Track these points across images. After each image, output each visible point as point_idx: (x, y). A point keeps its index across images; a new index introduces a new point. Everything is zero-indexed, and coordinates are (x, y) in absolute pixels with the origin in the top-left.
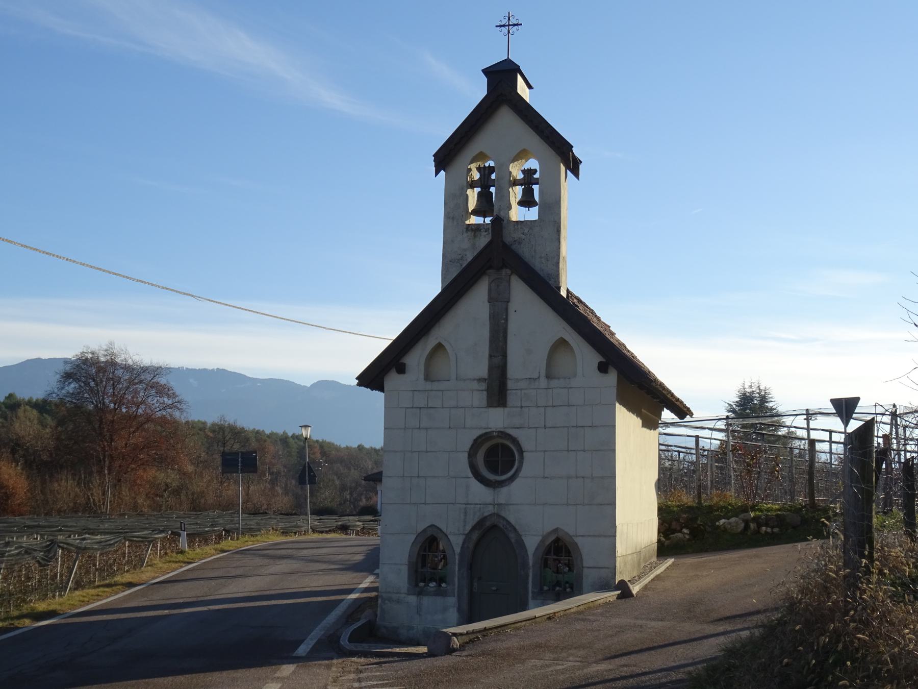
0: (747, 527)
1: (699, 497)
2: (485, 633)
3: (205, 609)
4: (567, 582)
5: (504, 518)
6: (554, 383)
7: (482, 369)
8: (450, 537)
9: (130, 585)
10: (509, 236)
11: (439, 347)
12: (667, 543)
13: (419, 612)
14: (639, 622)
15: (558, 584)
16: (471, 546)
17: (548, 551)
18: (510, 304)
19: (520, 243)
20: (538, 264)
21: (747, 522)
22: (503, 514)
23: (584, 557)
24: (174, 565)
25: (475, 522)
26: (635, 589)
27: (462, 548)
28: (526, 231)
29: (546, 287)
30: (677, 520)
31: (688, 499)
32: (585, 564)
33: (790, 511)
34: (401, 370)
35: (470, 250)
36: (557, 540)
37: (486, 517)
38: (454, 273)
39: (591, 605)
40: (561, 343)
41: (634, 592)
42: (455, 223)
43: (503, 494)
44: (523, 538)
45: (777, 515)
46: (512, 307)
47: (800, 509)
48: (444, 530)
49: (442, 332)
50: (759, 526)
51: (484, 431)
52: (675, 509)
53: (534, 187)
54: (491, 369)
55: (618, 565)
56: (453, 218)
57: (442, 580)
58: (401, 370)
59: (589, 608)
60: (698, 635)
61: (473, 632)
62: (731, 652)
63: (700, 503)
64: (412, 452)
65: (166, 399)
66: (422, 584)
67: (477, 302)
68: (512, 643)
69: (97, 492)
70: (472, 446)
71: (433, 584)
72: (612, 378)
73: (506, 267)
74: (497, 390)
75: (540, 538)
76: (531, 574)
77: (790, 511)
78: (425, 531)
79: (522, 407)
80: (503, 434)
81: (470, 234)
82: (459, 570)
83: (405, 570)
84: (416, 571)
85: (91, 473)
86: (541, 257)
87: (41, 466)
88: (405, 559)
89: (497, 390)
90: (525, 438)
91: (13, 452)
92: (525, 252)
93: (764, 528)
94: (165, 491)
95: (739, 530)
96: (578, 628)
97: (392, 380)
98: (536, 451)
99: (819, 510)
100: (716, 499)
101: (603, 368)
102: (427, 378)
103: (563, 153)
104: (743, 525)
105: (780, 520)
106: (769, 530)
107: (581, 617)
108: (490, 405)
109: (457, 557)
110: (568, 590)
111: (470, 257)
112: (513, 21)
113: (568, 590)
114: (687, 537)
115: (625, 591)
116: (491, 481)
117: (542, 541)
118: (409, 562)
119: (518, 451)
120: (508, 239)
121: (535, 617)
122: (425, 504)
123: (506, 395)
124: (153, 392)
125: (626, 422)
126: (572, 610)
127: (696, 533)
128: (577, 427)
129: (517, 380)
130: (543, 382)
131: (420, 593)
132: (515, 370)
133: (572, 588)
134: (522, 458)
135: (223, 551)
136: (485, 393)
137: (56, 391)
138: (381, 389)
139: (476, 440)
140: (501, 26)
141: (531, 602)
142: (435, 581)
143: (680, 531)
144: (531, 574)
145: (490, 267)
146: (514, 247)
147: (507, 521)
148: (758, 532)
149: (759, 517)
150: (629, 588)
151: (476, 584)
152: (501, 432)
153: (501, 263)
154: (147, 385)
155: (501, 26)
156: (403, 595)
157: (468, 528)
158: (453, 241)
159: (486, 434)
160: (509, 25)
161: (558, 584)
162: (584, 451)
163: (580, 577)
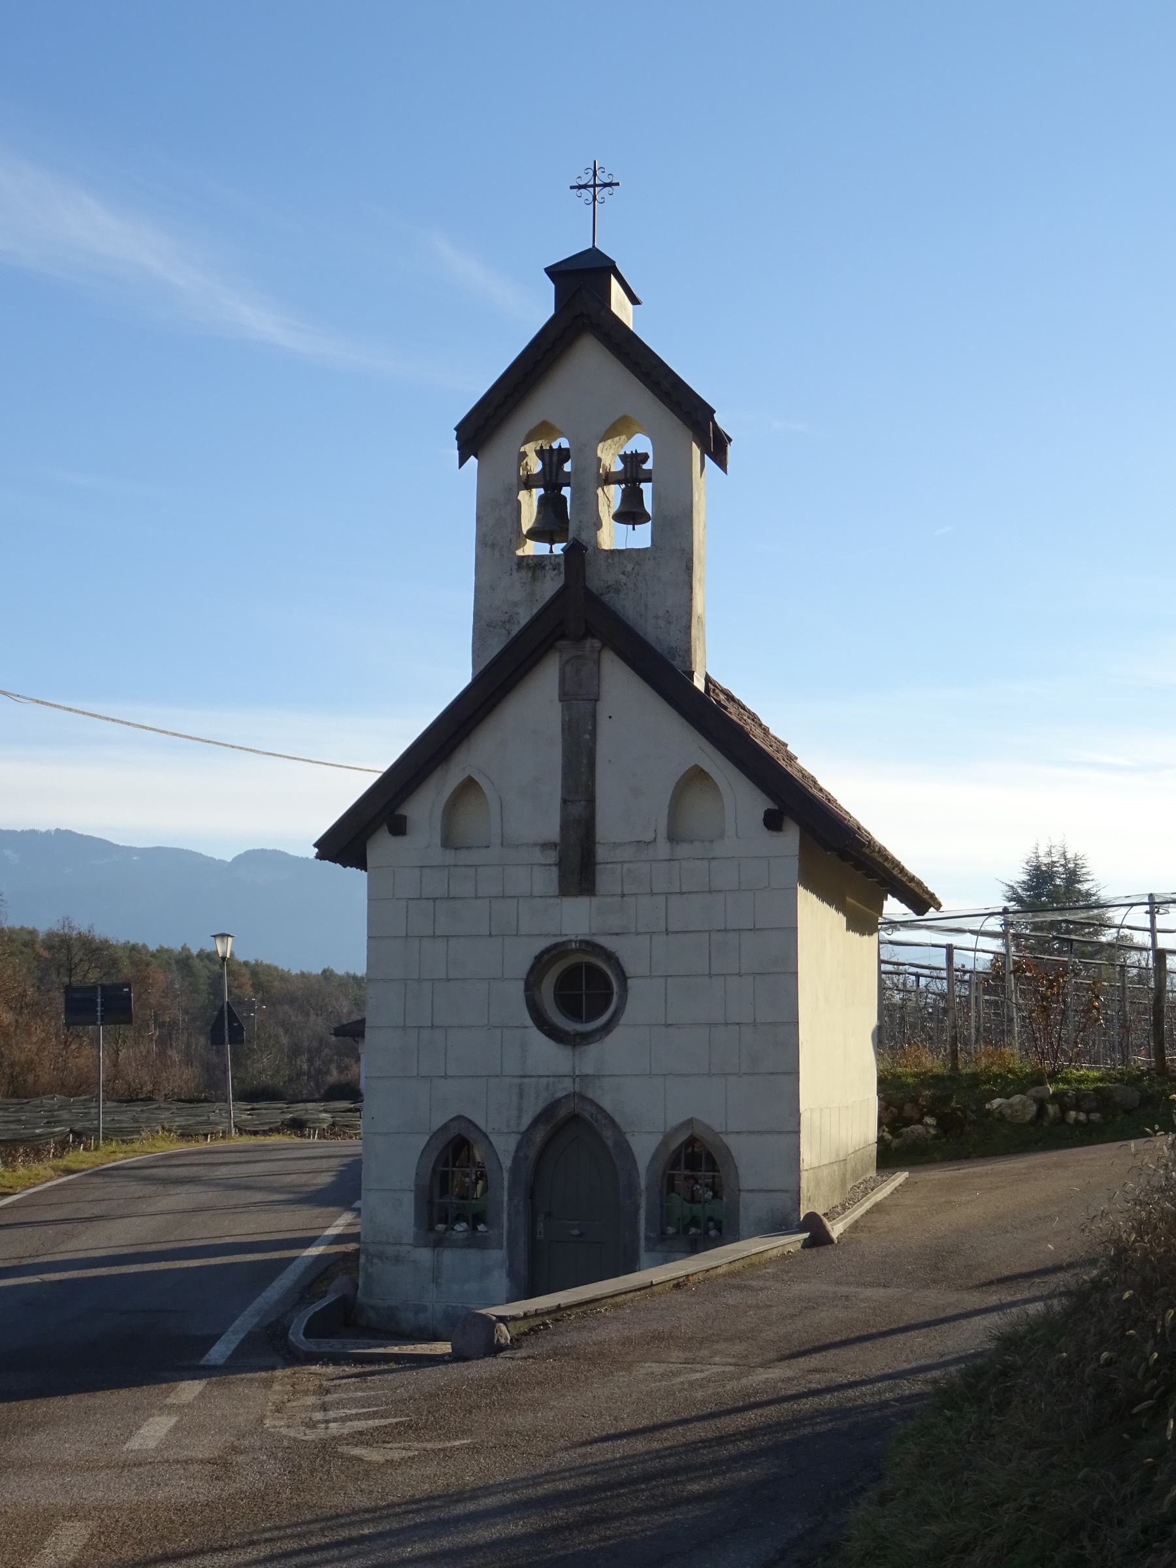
4: (710, 1219)
6: (683, 850)
7: (551, 829)
8: (492, 1138)
10: (598, 578)
11: (470, 784)
12: (896, 1143)
14: (844, 1290)
15: (694, 1222)
16: (532, 1154)
17: (674, 1163)
19: (618, 591)
20: (651, 631)
21: (1041, 1104)
22: (590, 1095)
25: (539, 1110)
26: (836, 1229)
28: (629, 568)
30: (914, 1101)
31: (933, 1062)
32: (744, 1185)
33: (1117, 1080)
34: (399, 828)
36: (692, 1141)
37: (558, 1101)
38: (496, 646)
39: (755, 1259)
40: (696, 776)
43: (592, 1057)
44: (628, 1137)
45: (1096, 1090)
46: (605, 708)
47: (1139, 1078)
49: (476, 757)
50: (1064, 1109)
52: (910, 1080)
53: (643, 486)
54: (565, 825)
55: (803, 1184)
57: (478, 1218)
58: (399, 828)
59: (752, 1265)
60: (950, 1312)
63: (955, 1068)
66: (440, 1227)
67: (539, 700)
68: (610, 1332)
71: (461, 1227)
72: (790, 839)
73: (593, 636)
74: (578, 862)
75: (660, 1138)
76: (643, 1203)
78: (445, 1127)
79: (623, 896)
80: (589, 946)
81: (526, 575)
82: (510, 1199)
84: (430, 1203)
86: (657, 617)
88: (409, 1182)
89: (578, 862)
92: (627, 606)
93: (1073, 1114)
95: (1028, 1117)
96: (730, 1302)
97: (382, 846)
98: (650, 977)
100: (984, 1061)
101: (773, 822)
102: (448, 842)
104: (1035, 1108)
105: (1102, 1100)
106: (1082, 1117)
107: (734, 1282)
108: (565, 891)
109: (506, 1176)
110: (713, 1233)
111: (524, 618)
112: (602, 178)
113: (713, 1233)
114: (933, 1131)
115: (817, 1236)
117: (664, 1143)
118: (417, 1186)
122: (445, 1077)
123: (593, 873)
125: (817, 921)
126: (720, 1271)
127: (948, 1124)
128: (726, 930)
129: (615, 845)
130: (663, 849)
131: (438, 1244)
133: (719, 1229)
135: (69, 1171)
136: (555, 869)
138: (362, 864)
139: (538, 959)
142: (466, 1220)
143: (920, 1121)
144: (643, 1203)
145: (563, 636)
148: (1061, 1120)
149: (1064, 1093)
150: (824, 1227)
152: (588, 943)
153: (581, 629)
156: (409, 1248)
157: (526, 1121)
159: (556, 945)
161: (694, 1222)
162: (740, 975)
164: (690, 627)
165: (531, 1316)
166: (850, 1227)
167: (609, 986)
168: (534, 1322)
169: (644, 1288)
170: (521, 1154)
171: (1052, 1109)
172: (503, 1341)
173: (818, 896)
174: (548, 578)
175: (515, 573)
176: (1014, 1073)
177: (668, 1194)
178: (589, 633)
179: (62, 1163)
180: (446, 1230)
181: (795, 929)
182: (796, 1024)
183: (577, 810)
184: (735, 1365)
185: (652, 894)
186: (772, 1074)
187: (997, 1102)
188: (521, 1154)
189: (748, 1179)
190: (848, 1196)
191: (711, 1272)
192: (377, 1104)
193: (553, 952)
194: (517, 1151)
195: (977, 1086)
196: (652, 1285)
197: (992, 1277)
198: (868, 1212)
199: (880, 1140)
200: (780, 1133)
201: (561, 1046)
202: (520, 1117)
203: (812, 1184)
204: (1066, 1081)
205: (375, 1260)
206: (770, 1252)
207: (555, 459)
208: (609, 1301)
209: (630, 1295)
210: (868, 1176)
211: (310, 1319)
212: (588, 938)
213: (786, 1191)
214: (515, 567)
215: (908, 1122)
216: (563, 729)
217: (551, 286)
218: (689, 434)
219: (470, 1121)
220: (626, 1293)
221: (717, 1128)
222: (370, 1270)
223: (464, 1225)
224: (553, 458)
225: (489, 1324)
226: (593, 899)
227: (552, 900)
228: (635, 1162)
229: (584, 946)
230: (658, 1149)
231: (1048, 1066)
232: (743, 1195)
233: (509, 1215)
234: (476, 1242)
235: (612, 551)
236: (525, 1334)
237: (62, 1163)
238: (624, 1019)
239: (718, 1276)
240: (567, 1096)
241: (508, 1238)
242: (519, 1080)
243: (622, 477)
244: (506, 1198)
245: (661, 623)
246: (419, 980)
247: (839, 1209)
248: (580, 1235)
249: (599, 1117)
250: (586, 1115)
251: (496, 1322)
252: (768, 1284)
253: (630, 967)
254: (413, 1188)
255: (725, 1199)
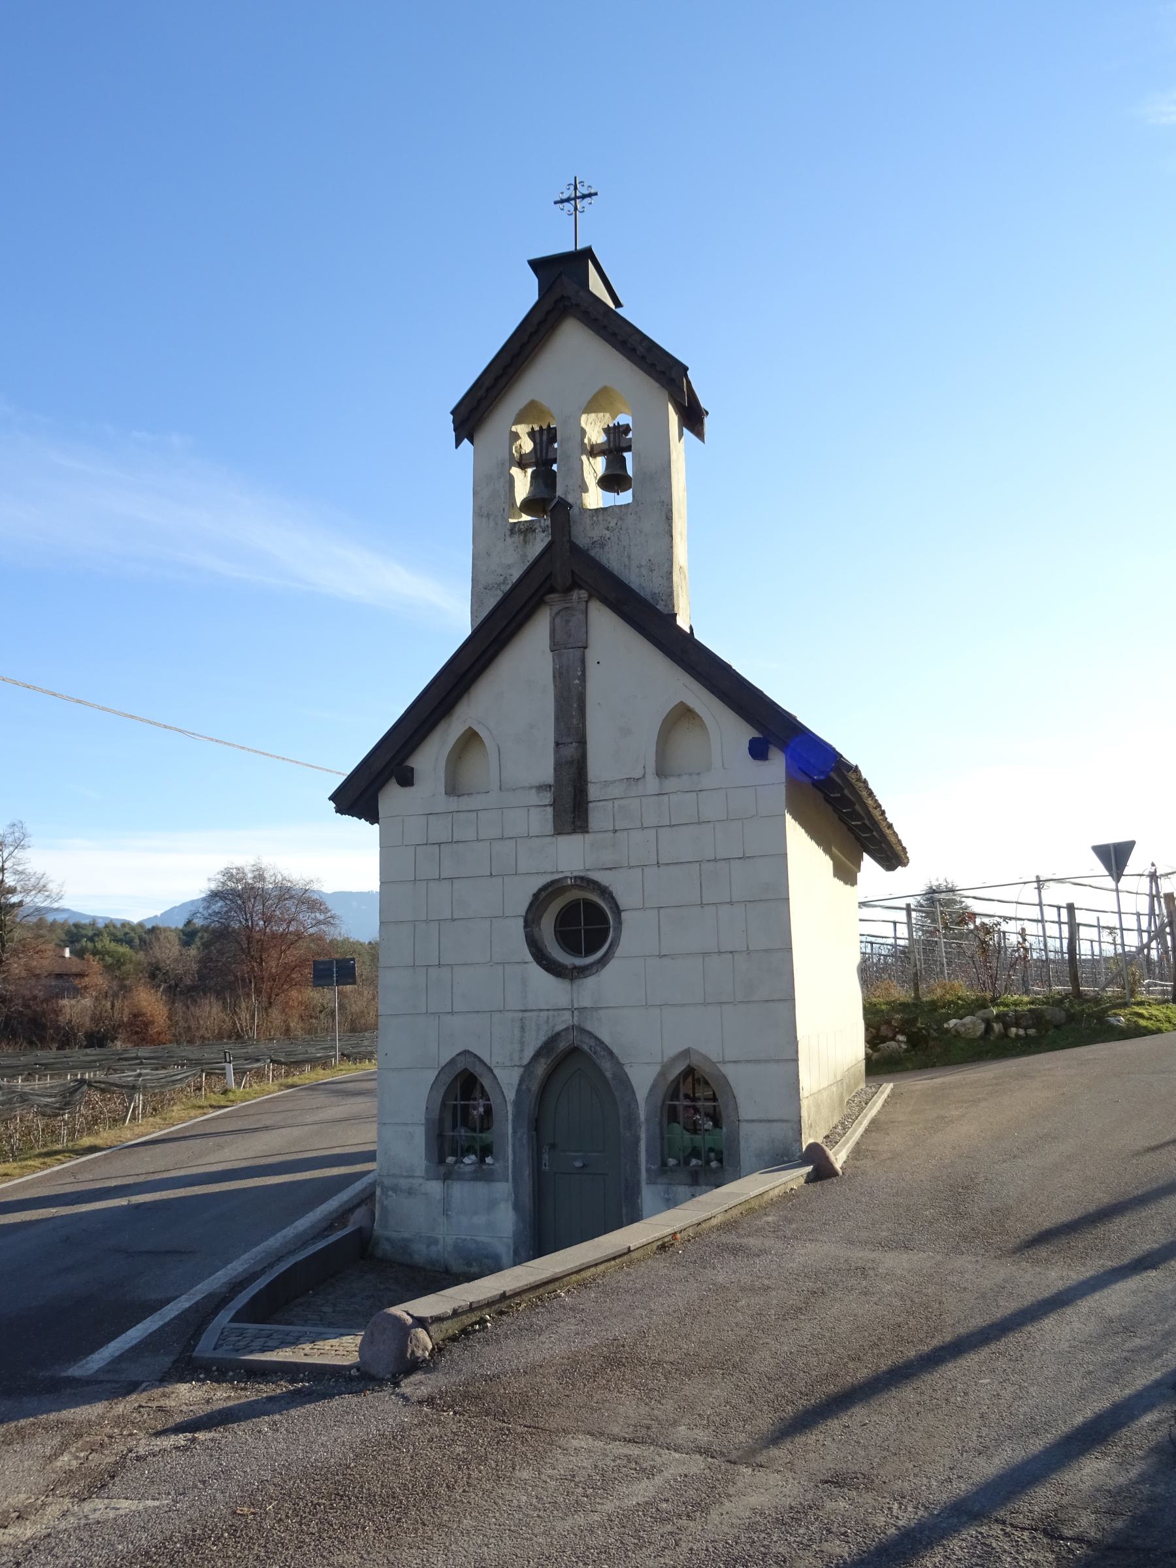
0: (988, 1029)
1: (917, 990)
2: (503, 1306)
3: (123, 1202)
4: (711, 1150)
5: (590, 1034)
6: (671, 784)
7: (546, 771)
8: (496, 1071)
9: (93, 1149)
10: (584, 535)
11: (471, 738)
12: (875, 1055)
13: (445, 1212)
14: (860, 1255)
15: (695, 1152)
16: (535, 1087)
17: (674, 1092)
18: (587, 651)
19: (602, 546)
20: (635, 579)
21: (988, 1023)
22: (589, 1027)
23: (741, 1100)
24: (193, 1113)
25: (539, 1044)
26: (839, 1157)
27: (518, 1091)
28: (612, 524)
29: (652, 620)
30: (888, 1023)
31: (901, 993)
32: (744, 1114)
33: (1044, 1003)
34: (407, 779)
35: (513, 562)
36: (690, 1072)
37: (558, 1034)
38: (491, 603)
39: (753, 1204)
40: (683, 714)
41: (838, 1165)
42: (492, 524)
43: (589, 989)
44: (627, 1069)
45: (1030, 1010)
46: (592, 656)
47: (1061, 1001)
48: (486, 1060)
49: (473, 711)
50: (1007, 1027)
51: (548, 879)
52: (884, 1007)
53: (625, 454)
54: (558, 766)
55: (804, 1113)
56: (488, 516)
57: (486, 1150)
58: (407, 779)
59: (751, 1210)
60: (1007, 1307)
61: (472, 1308)
62: (1138, 1417)
63: (917, 997)
64: (427, 921)
65: (318, 915)
66: (450, 1160)
68: (550, 1344)
69: (244, 1015)
70: (531, 905)
71: (470, 1159)
72: (777, 766)
73: (581, 588)
74: (571, 803)
75: (658, 1068)
76: (643, 1136)
77: (1047, 1003)
78: (452, 1062)
79: (615, 831)
80: (584, 882)
81: (518, 539)
82: (515, 1132)
83: (419, 1136)
84: (441, 1136)
85: (238, 997)
86: (640, 566)
87: (180, 991)
88: (420, 1116)
89: (571, 803)
90: (624, 888)
91: (153, 976)
92: (612, 559)
93: (1014, 1030)
94: (321, 1012)
95: (979, 1034)
96: (720, 1279)
97: (392, 798)
98: (644, 909)
99: (1088, 1001)
100: (939, 992)
101: (758, 751)
102: (453, 789)
103: (667, 373)
104: (983, 1026)
105: (1036, 1018)
106: (1021, 1032)
107: (731, 1239)
108: (559, 831)
109: (510, 1108)
110: (714, 1164)
111: (516, 574)
112: (582, 190)
113: (714, 1164)
114: (904, 1046)
115: (822, 1171)
116: (564, 967)
117: (662, 1074)
118: (427, 1119)
119: (613, 912)
120: (582, 541)
121: (629, 1251)
122: (452, 1013)
123: (586, 810)
124: (304, 907)
125: (805, 857)
126: (714, 1222)
127: (916, 1041)
128: (715, 860)
129: (606, 784)
130: (652, 784)
131: (448, 1176)
132: (601, 766)
133: (720, 1161)
134: (619, 922)
135: (292, 1086)
136: (550, 810)
137: (201, 910)
138: (373, 818)
139: (536, 896)
140: (562, 201)
141: (648, 1194)
142: (475, 1153)
143: (893, 1039)
144: (643, 1136)
145: (552, 590)
146: (592, 553)
147: (596, 1038)
148: (1005, 1035)
149: (1005, 1015)
150: (827, 1158)
151: (546, 1157)
152: (582, 878)
153: (570, 576)
154: (299, 900)
155: (562, 201)
156: (421, 1181)
157: (529, 1053)
158: (488, 554)
159: (553, 882)
160: (576, 198)
161: (695, 1152)
162: (731, 903)
163: (734, 1140)
164: (671, 573)
165: (464, 1313)
166: (852, 1152)
167: (606, 921)
168: (467, 1320)
169: (620, 1256)
170: (524, 1087)
171: (997, 1027)
172: (419, 1353)
173: (807, 831)
174: (538, 539)
175: (508, 539)
176: (963, 1000)
177: (669, 1123)
178: (575, 585)
179: (290, 1080)
180: (456, 1162)
181: (784, 855)
182: (789, 950)
183: (570, 751)
184: (705, 1451)
185: (643, 828)
186: (767, 1001)
187: (953, 1022)
188: (524, 1087)
189: (746, 1110)
190: (847, 1111)
191: (703, 1225)
192: (394, 1040)
193: (550, 889)
194: (520, 1084)
195: (936, 1010)
196: (629, 1251)
197: (1033, 1231)
198: (867, 1131)
199: (867, 1054)
200: (778, 1061)
201: (559, 980)
202: (522, 1051)
203: (813, 1109)
204: (1007, 1005)
205: (390, 1193)
206: (771, 1194)
207: (545, 438)
208: (574, 1278)
209: (602, 1267)
210: (859, 1088)
211: (296, 1264)
212: (582, 874)
213: (787, 1121)
214: (508, 533)
215: (884, 1039)
216: (554, 677)
217: (534, 281)
218: (664, 395)
219: (476, 1056)
220: (596, 1265)
221: (714, 1057)
222: (385, 1203)
223: (473, 1157)
224: (545, 438)
225: (402, 1331)
226: (587, 836)
227: (548, 839)
228: (633, 1092)
229: (578, 882)
230: (656, 1080)
231: (989, 995)
232: (743, 1126)
233: (513, 1146)
234: (483, 1175)
235: (597, 510)
236: (454, 1339)
237: (290, 1080)
238: (619, 952)
239: (711, 1229)
240: (567, 1029)
241: (513, 1172)
242: (521, 1015)
243: (606, 447)
244: (510, 1131)
245: (644, 571)
246: (427, 921)
247: (839, 1130)
248: (584, 1166)
249: (598, 1049)
250: (586, 1048)
251: (414, 1326)
252: (768, 1243)
253: (623, 901)
254: (423, 1121)
255: (724, 1129)
